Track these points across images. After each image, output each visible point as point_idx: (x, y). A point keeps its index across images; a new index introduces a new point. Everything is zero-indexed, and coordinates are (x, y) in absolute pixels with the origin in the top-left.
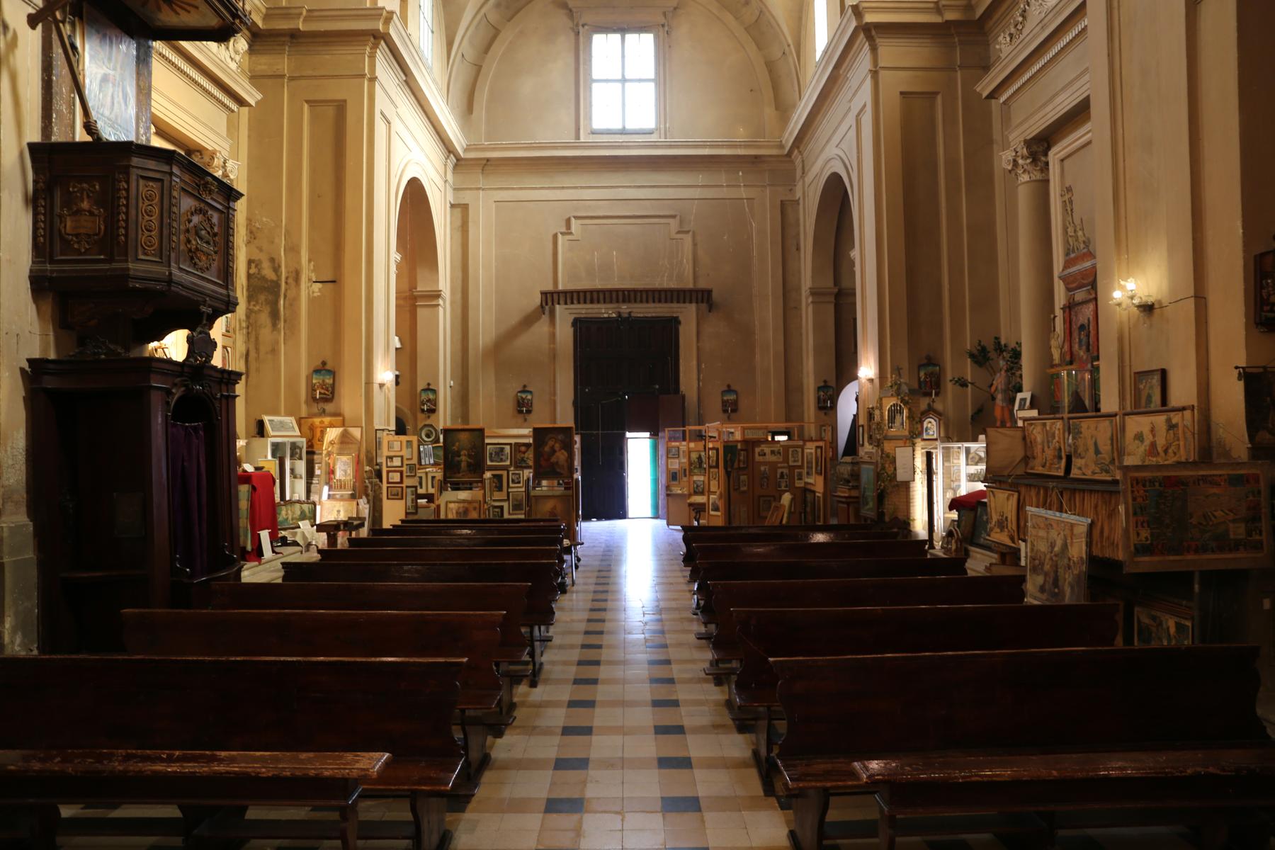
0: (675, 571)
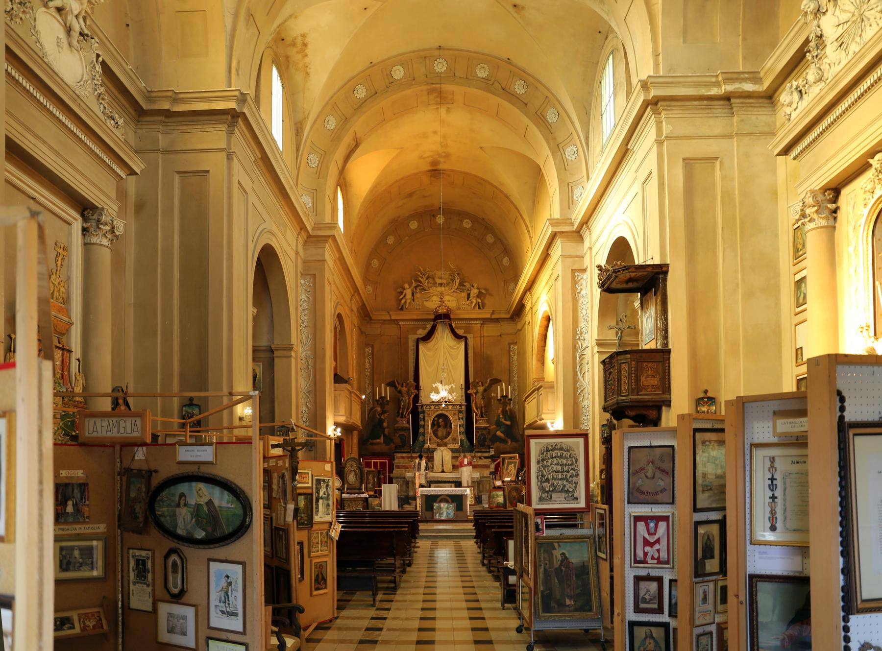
0: (457, 587)
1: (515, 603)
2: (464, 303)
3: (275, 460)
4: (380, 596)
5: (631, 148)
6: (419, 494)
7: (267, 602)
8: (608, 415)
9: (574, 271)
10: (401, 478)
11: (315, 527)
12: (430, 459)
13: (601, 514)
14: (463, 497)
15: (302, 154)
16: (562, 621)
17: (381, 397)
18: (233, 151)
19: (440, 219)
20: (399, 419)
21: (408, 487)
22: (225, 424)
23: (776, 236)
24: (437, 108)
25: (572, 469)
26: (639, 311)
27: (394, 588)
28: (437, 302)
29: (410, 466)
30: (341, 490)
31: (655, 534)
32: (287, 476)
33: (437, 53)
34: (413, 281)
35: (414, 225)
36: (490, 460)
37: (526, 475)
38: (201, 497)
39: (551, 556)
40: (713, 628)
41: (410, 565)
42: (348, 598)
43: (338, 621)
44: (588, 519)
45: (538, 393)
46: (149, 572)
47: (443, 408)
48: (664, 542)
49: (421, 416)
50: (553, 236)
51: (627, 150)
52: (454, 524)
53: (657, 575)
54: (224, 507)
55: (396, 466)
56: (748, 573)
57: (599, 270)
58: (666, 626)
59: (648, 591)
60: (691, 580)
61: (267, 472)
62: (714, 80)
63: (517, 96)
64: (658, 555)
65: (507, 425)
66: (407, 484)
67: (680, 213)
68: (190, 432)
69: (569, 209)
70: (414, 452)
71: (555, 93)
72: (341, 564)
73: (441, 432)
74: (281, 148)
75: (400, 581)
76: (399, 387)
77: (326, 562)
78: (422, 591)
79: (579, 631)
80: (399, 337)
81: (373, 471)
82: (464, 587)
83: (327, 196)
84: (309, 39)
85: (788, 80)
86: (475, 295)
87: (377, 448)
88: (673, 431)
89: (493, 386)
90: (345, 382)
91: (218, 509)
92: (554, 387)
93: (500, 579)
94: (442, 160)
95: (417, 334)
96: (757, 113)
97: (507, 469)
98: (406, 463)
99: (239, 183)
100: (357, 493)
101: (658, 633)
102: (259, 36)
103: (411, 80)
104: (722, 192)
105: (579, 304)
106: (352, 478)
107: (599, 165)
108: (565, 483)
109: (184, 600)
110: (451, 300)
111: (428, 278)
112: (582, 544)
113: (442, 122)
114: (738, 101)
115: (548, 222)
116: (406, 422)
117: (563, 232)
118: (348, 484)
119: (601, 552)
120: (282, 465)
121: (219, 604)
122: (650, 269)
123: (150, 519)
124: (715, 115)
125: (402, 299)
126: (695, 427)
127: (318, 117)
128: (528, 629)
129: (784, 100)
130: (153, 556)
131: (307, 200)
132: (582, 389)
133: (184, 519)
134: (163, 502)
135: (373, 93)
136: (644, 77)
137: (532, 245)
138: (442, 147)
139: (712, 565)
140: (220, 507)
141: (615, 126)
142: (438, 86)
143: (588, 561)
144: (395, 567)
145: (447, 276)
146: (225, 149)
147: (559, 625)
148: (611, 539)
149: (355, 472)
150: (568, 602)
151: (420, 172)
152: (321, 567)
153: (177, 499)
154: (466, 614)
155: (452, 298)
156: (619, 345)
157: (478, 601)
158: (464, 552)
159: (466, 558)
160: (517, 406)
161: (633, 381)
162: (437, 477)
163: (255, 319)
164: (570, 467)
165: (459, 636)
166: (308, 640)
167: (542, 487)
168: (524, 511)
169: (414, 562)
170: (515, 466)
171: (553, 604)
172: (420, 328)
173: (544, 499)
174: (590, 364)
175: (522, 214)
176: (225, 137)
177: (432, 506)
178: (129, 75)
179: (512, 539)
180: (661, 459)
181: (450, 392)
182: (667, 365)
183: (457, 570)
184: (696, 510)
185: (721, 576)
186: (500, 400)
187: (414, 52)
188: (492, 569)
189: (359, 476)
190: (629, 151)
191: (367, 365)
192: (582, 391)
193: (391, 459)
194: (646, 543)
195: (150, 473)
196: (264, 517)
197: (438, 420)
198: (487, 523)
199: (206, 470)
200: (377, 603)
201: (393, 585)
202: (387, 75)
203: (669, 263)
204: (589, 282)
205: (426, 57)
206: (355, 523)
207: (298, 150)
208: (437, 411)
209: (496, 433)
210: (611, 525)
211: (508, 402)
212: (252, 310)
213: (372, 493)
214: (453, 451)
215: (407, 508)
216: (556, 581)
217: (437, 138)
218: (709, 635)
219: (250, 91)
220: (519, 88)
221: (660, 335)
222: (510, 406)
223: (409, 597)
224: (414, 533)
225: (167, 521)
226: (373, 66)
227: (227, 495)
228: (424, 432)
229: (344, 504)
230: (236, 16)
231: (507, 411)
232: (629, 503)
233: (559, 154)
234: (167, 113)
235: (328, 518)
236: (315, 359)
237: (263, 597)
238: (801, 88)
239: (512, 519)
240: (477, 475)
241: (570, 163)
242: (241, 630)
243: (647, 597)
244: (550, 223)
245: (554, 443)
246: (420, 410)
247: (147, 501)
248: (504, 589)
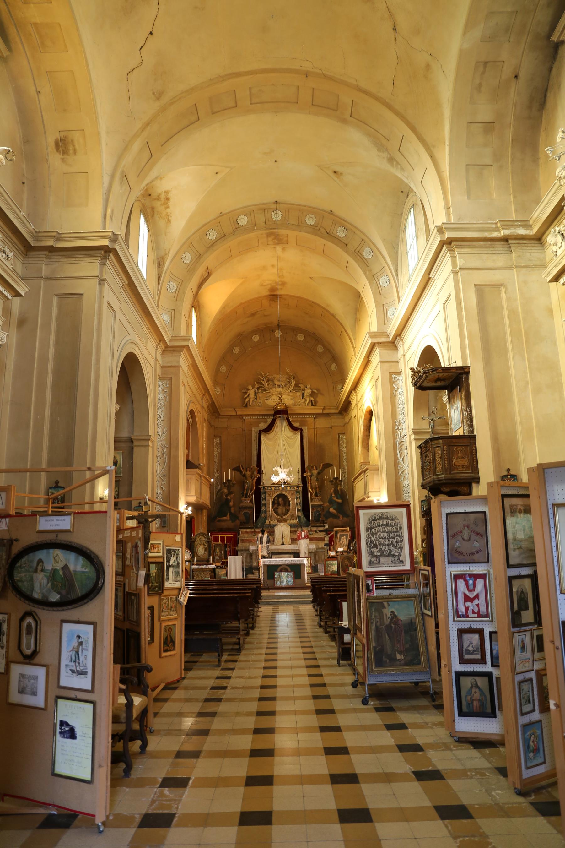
1: (350, 660)
2: (299, 401)
3: (129, 531)
4: (225, 657)
5: (433, 277)
6: (261, 564)
7: (115, 662)
8: (426, 492)
9: (391, 374)
10: (246, 550)
11: (165, 593)
12: (271, 533)
13: (425, 576)
14: (301, 566)
15: (163, 281)
16: (393, 675)
17: (227, 480)
18: (104, 277)
19: (278, 334)
20: (243, 499)
21: (252, 559)
22: (87, 500)
23: (555, 344)
24: (275, 248)
25: (397, 536)
26: (448, 405)
27: (238, 649)
28: (277, 401)
29: (254, 540)
30: (191, 562)
31: (474, 590)
32: (140, 545)
33: (274, 206)
34: (256, 383)
35: (256, 338)
36: (324, 533)
37: (357, 545)
38: (58, 562)
39: (381, 614)
40: (533, 675)
41: (253, 628)
42: (195, 659)
43: (185, 682)
44: (413, 580)
45: (365, 475)
46: (4, 635)
47: (283, 488)
48: (482, 597)
49: (263, 496)
50: (373, 346)
51: (430, 278)
52: (293, 591)
53: (478, 628)
54: (79, 571)
56: (561, 620)
57: (412, 372)
58: (489, 675)
59: (471, 643)
60: (509, 630)
61: (121, 543)
62: (494, 226)
63: (340, 239)
64: (478, 609)
65: (338, 503)
66: (251, 556)
67: (476, 327)
68: (52, 508)
69: (385, 324)
70: (257, 527)
71: (369, 236)
72: (188, 628)
73: (281, 509)
74: (145, 277)
75: (244, 643)
76: (244, 472)
77: (175, 625)
78: (264, 651)
79: (410, 684)
80: (244, 429)
81: (220, 545)
82: (302, 647)
83: (183, 316)
84: (171, 195)
85: (552, 227)
86: (309, 394)
87: (224, 525)
88: (484, 499)
89: (326, 469)
90: (196, 467)
91: (73, 573)
92: (378, 470)
93: (336, 639)
94: (279, 287)
95: (259, 427)
96: (530, 251)
97: (340, 540)
99: (108, 303)
101: (482, 682)
102: (130, 191)
103: (253, 226)
104: (509, 311)
105: (397, 400)
106: (201, 550)
107: (407, 290)
108: (392, 548)
109: (36, 660)
110: (288, 400)
111: (268, 381)
112: (409, 602)
113: (279, 258)
114: (514, 241)
115: (368, 335)
116: (250, 502)
117: (380, 343)
118: (198, 556)
119: (426, 609)
120: (135, 535)
121: (70, 664)
122: (454, 371)
123: (8, 584)
124: (497, 252)
125: (246, 398)
126: (503, 493)
127: (177, 253)
128: (363, 684)
129: (550, 241)
130: (9, 619)
131: (166, 318)
132: (402, 470)
133: (40, 583)
134: (21, 568)
135: (222, 236)
136: (439, 224)
137: (355, 353)
138: (279, 277)
139: (528, 616)
140: (75, 571)
141: (419, 261)
142: (275, 230)
143: (415, 618)
144: (239, 630)
145: (284, 379)
146: (98, 276)
147: (390, 678)
148: (435, 599)
149: (204, 545)
150: (398, 656)
151: (261, 297)
152: (170, 630)
153: (35, 565)
154: (305, 671)
155: (288, 397)
156: (432, 433)
157: (316, 659)
158: (302, 615)
159: (305, 621)
160: (347, 487)
161: (446, 462)
162: (278, 549)
163: (118, 413)
164: (396, 534)
165: (298, 692)
166: (156, 700)
167: (372, 552)
168: (356, 574)
169: (257, 625)
170: (346, 538)
171: (384, 659)
172: (262, 421)
173: (373, 562)
174: (408, 449)
175: (346, 329)
176: (99, 267)
177: (274, 575)
178: (21, 219)
179: (346, 601)
180: (475, 523)
181: (289, 474)
182: (474, 448)
183: (297, 631)
184: (509, 566)
185: (536, 626)
186: (332, 481)
187: (256, 205)
188: (328, 630)
189: (208, 549)
190: (431, 279)
191: (216, 453)
192: (402, 472)
193: (237, 534)
194: (467, 598)
195: (11, 542)
196: (116, 583)
197: (278, 499)
198: (323, 587)
199: (63, 538)
200: (222, 664)
201: (237, 647)
202: (234, 222)
203: (469, 365)
204: (404, 382)
205: (265, 209)
206: (203, 590)
207: (159, 278)
208: (277, 492)
209: (329, 510)
210: (435, 587)
211: (339, 483)
212: (115, 406)
213: (219, 564)
214: (292, 526)
215: (251, 577)
216: (387, 637)
217: (275, 271)
218: (530, 682)
219: (122, 233)
220: (340, 232)
221: (466, 423)
222: (341, 486)
223: (252, 658)
224: (256, 598)
225: (24, 586)
226: (223, 215)
227: (81, 560)
228: (266, 510)
229: (193, 574)
230: (112, 177)
231: (338, 491)
232: (449, 563)
233: (375, 282)
234: (51, 249)
235: (178, 585)
237: (112, 656)
238: (563, 232)
239: (346, 584)
240: (313, 547)
241: (384, 289)
242: (89, 688)
243: (470, 648)
244: (369, 336)
245: (380, 513)
246: (262, 491)
247: (7, 567)
248: (339, 647)
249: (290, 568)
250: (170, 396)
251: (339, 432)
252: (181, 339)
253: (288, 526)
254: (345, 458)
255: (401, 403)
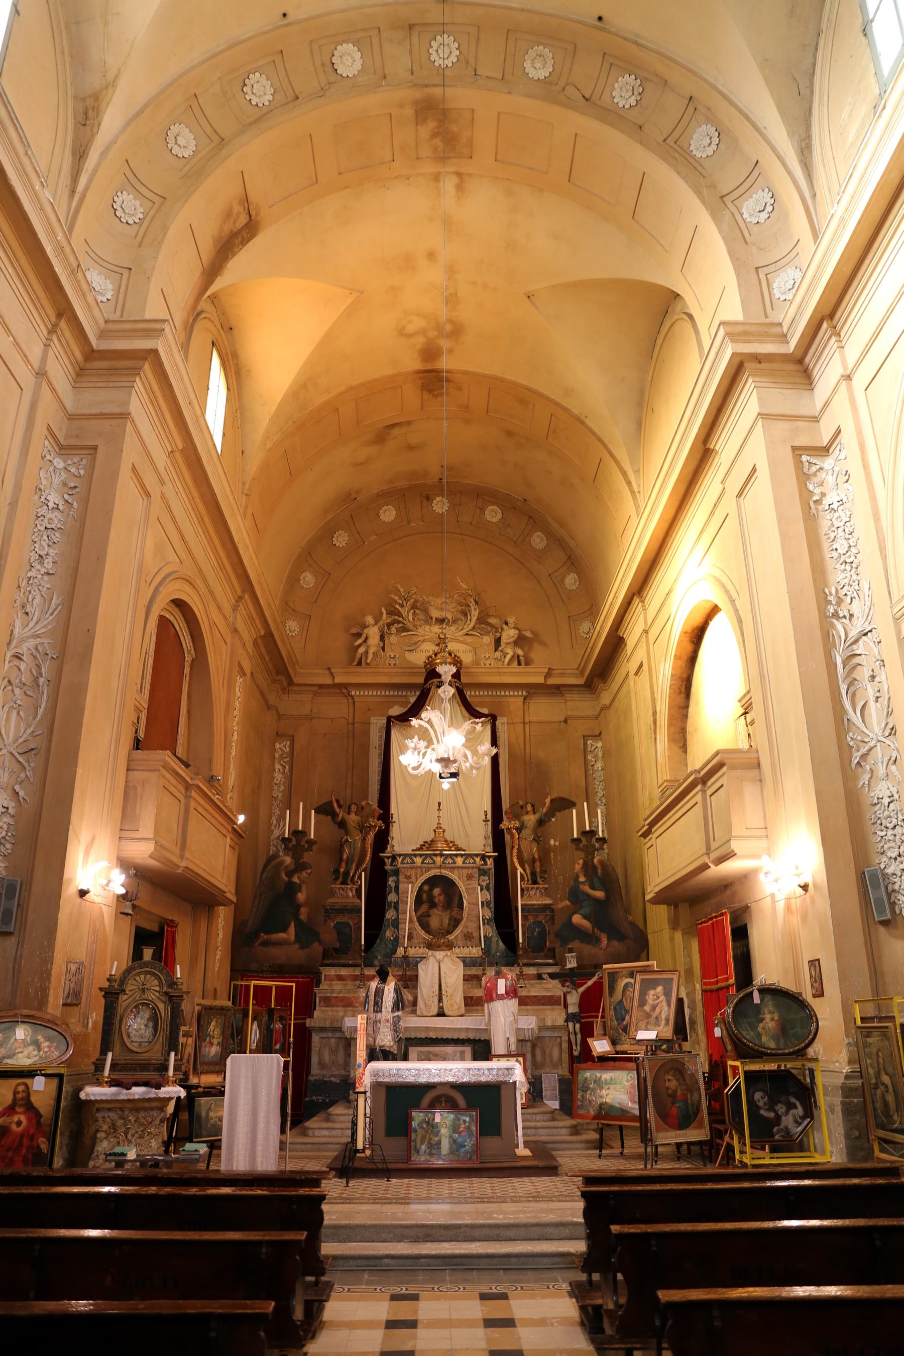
9: (797, 451)
12: (409, 981)
14: (503, 1092)
20: (337, 886)
49: (391, 882)
55: (321, 998)
65: (596, 900)
73: (438, 918)
76: (341, 814)
80: (351, 721)
86: (512, 639)
87: (279, 955)
94: (444, 344)
97: (642, 1003)
98: (349, 991)
100: (146, 1084)
113: (447, 222)
132: (864, 750)
137: (637, 506)
142: (438, 91)
162: (427, 1029)
177: (408, 1119)
186: (578, 840)
191: (278, 777)
192: (864, 756)
197: (431, 889)
202: (323, 64)
208: (429, 869)
211: (597, 845)
214: (468, 963)
217: (434, 275)
228: (398, 918)
231: (594, 867)
233: (727, 213)
236: (60, 660)
240: (529, 1023)
244: (727, 334)
246: (388, 867)
249: (463, 1094)
250: (85, 503)
251: (586, 733)
252: (135, 330)
253: (458, 960)
254: (600, 795)
255: (841, 533)
